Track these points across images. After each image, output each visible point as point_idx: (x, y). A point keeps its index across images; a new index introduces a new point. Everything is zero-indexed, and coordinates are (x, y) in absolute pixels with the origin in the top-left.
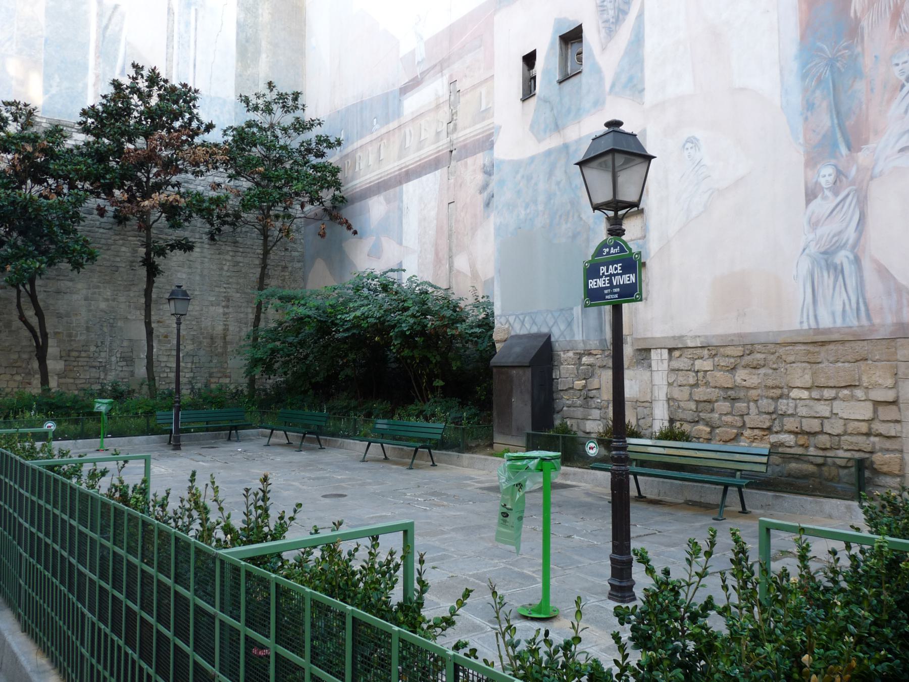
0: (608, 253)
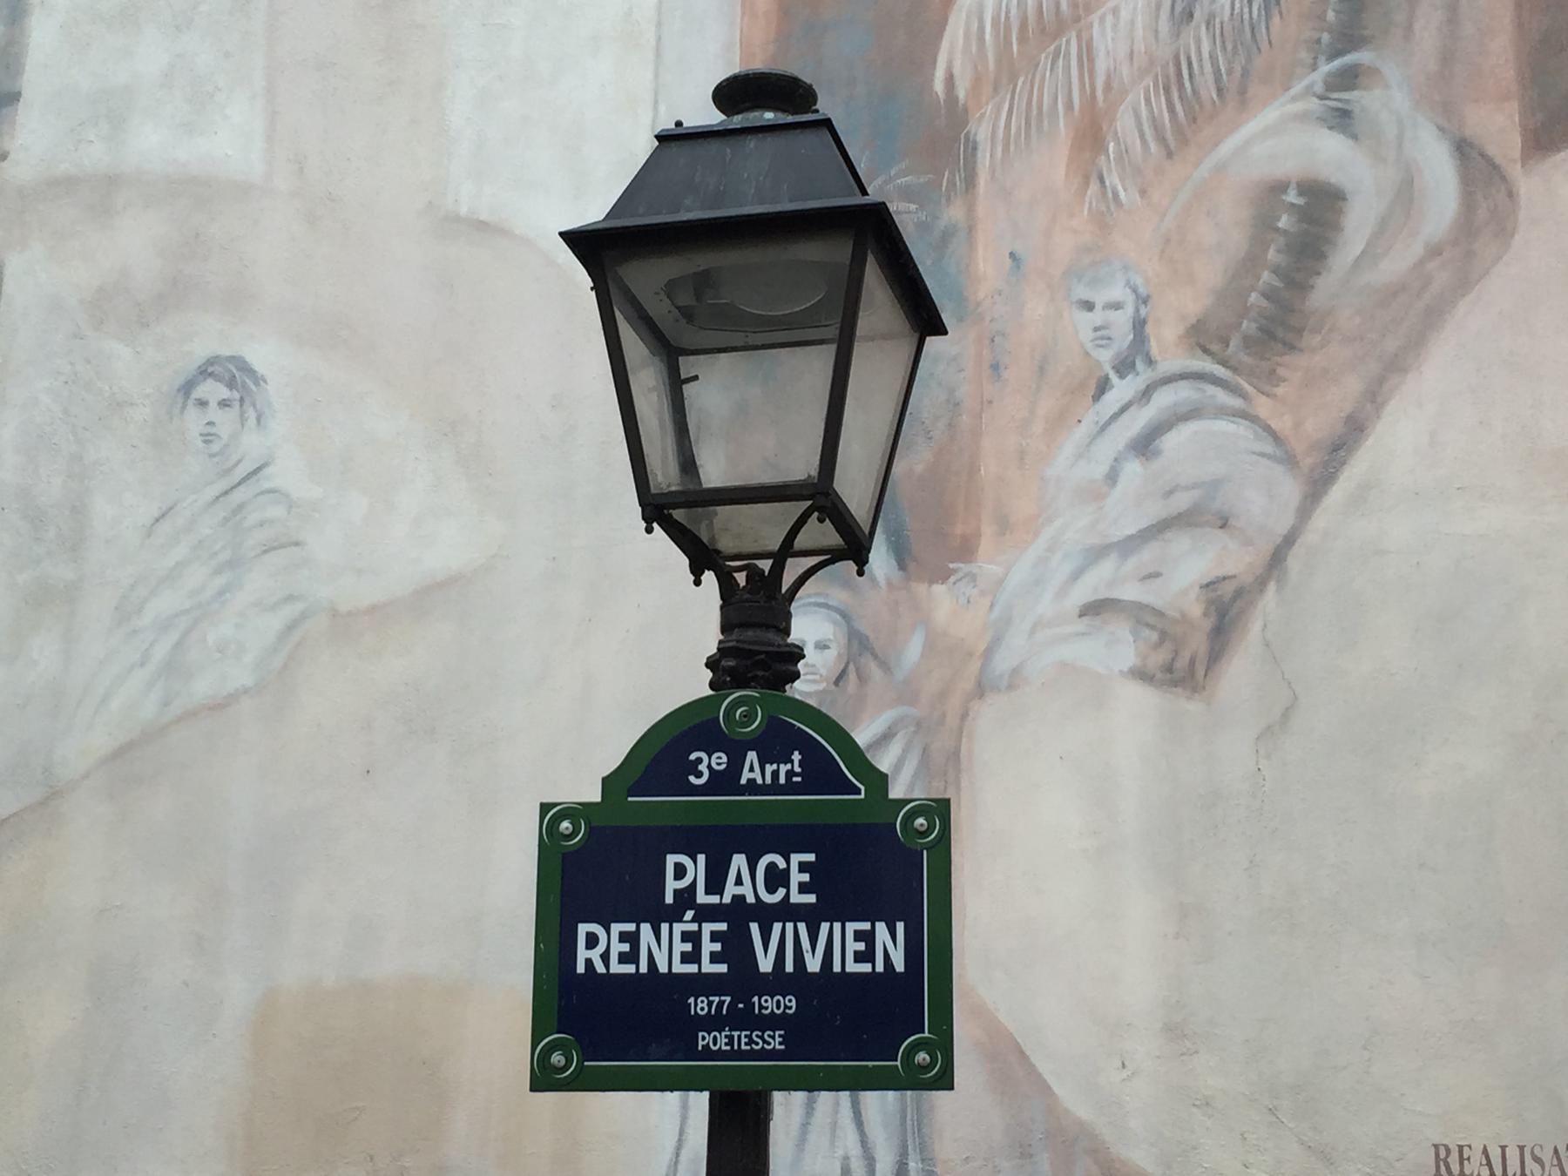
0: (724, 781)
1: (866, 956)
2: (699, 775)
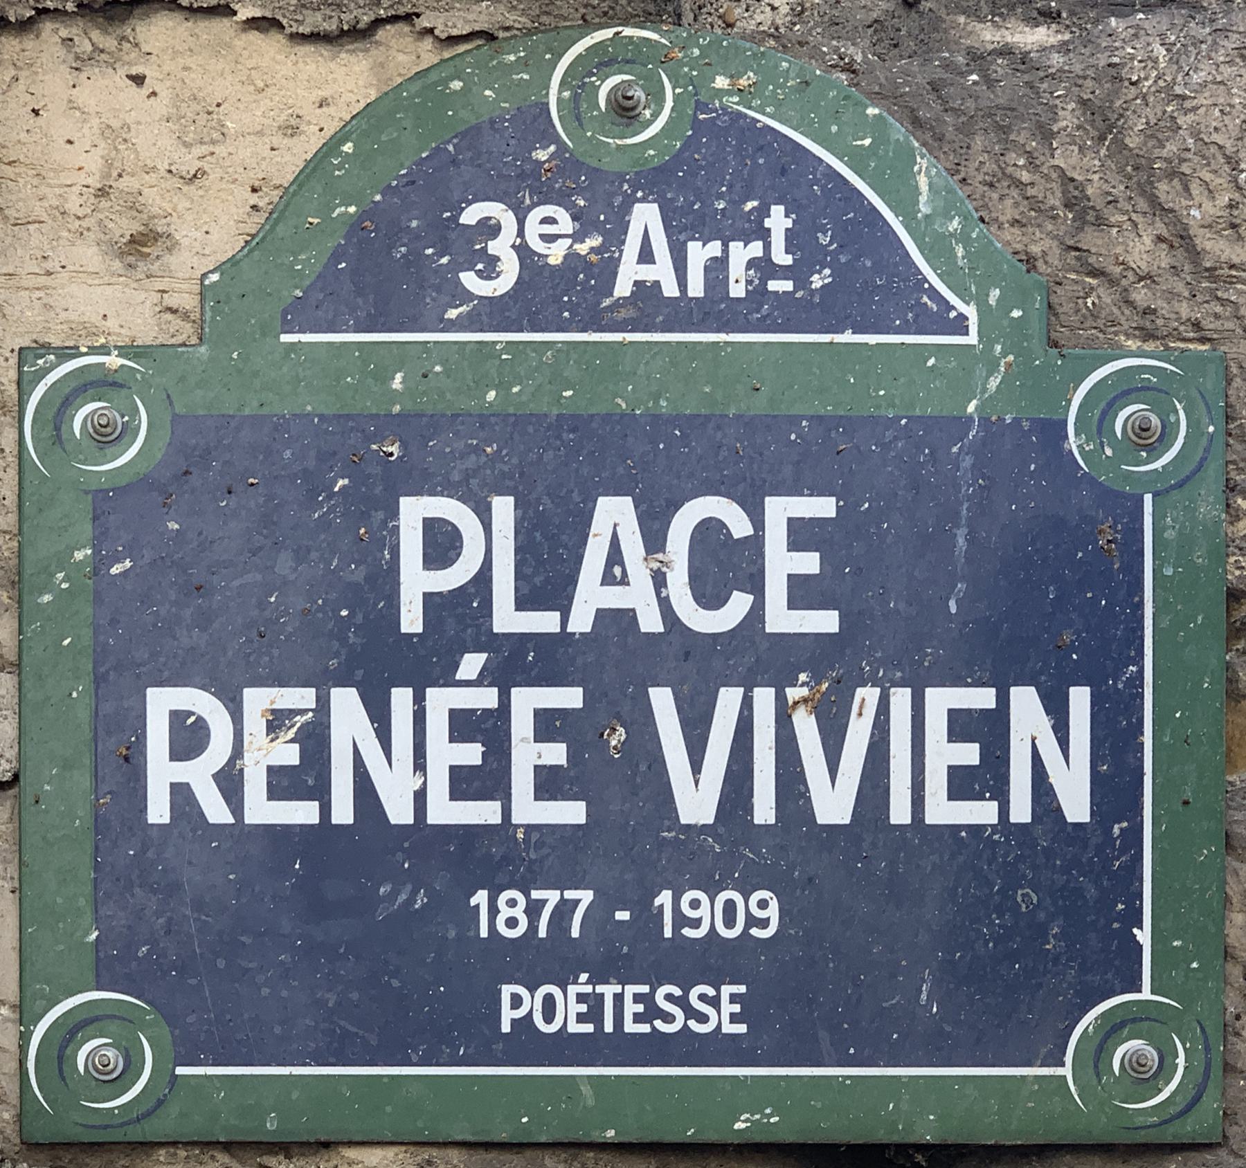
0: (548, 293)
1: (982, 780)
2: (490, 269)
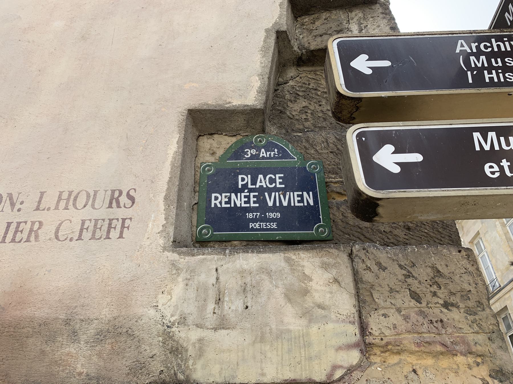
0: (253, 157)
